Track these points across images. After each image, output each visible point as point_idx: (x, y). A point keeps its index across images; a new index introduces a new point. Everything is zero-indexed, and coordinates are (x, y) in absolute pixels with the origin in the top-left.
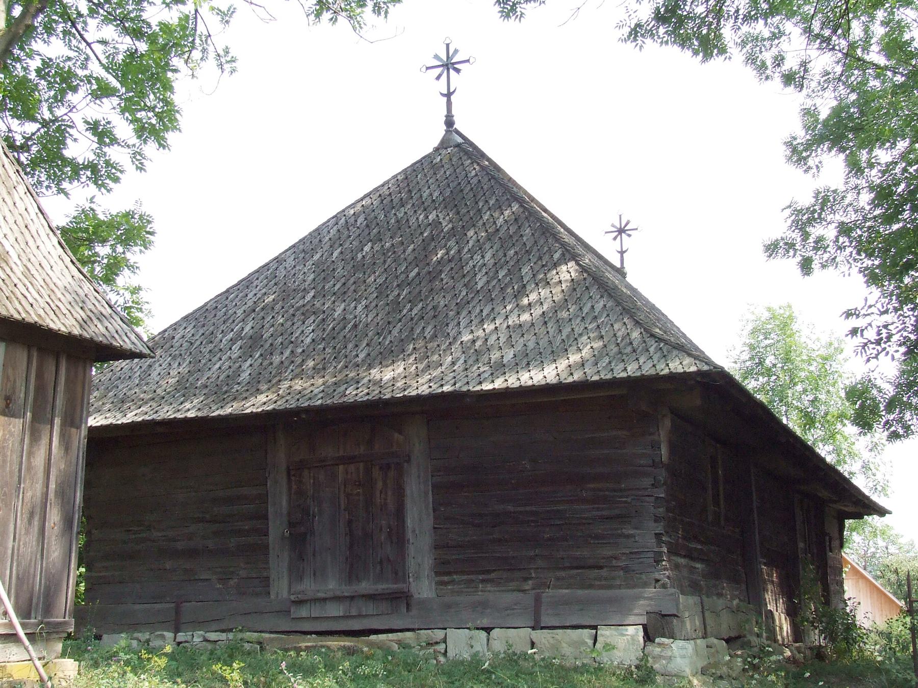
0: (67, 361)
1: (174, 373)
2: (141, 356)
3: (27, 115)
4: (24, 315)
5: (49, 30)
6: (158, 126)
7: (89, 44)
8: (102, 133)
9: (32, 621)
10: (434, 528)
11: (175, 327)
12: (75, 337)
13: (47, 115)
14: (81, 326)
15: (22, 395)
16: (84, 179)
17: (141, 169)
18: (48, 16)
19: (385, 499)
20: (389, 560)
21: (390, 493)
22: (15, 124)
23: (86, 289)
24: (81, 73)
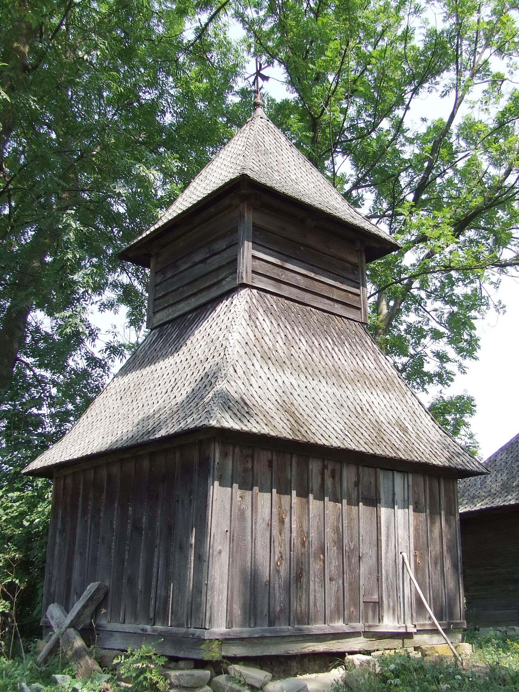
0: (444, 481)
1: (499, 479)
2: (482, 473)
3: (403, 352)
4: (420, 459)
5: (408, 309)
6: (469, 349)
7: (428, 313)
8: (442, 357)
9: (444, 622)
11: (496, 455)
12: (447, 467)
13: (412, 352)
14: (449, 461)
15: (423, 501)
16: (435, 382)
17: (464, 373)
18: (407, 302)
22: (397, 359)
23: (448, 441)
24: (426, 328)
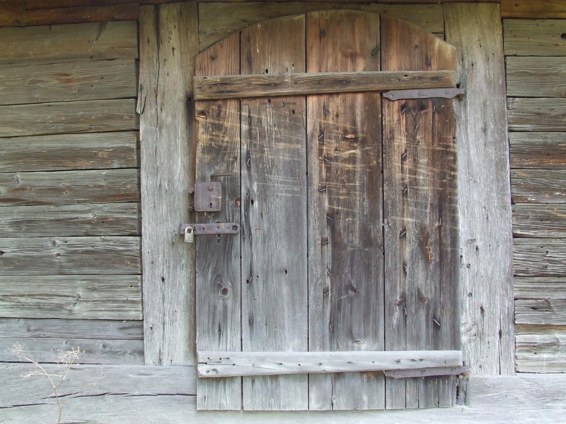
10: (515, 236)
19: (414, 172)
20: (421, 298)
21: (423, 160)
